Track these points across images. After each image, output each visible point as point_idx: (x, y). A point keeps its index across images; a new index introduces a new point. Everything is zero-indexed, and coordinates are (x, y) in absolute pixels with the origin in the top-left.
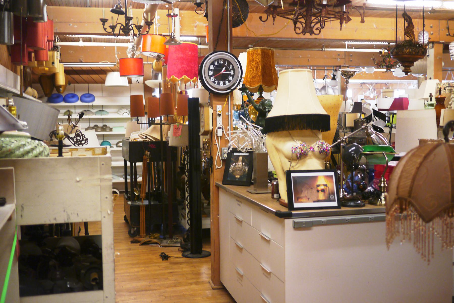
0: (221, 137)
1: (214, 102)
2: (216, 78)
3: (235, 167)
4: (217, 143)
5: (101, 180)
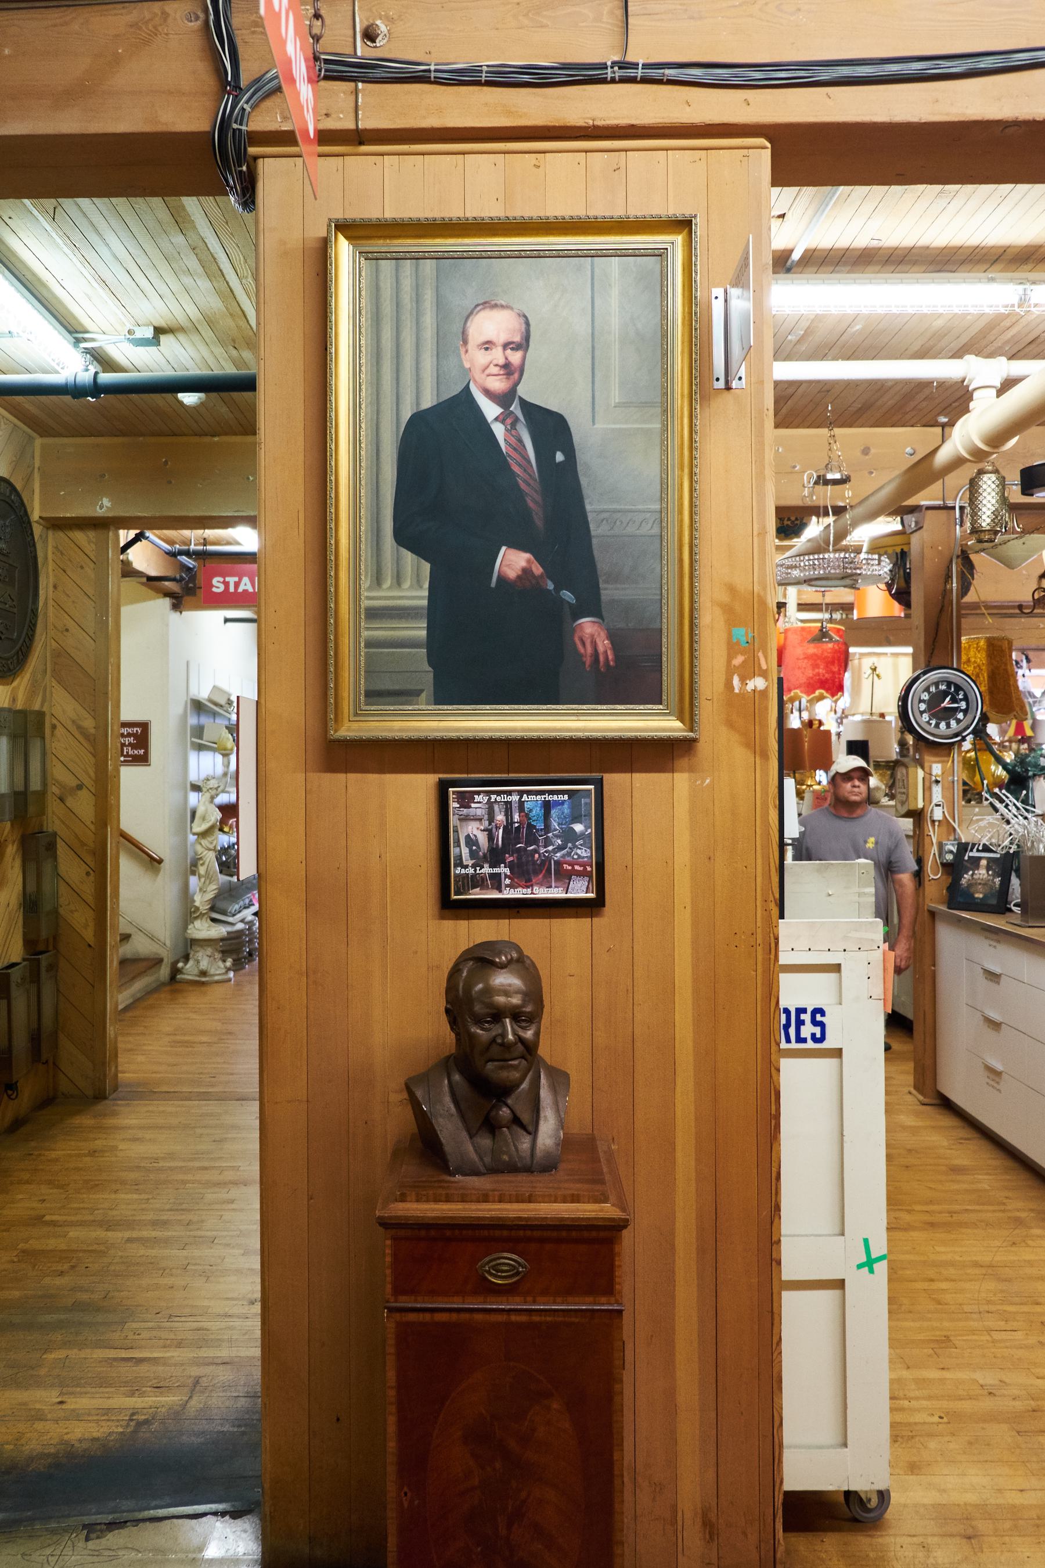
0: (939, 821)
1: (928, 758)
2: (933, 716)
3: (973, 879)
4: (931, 833)
5: (860, 895)
